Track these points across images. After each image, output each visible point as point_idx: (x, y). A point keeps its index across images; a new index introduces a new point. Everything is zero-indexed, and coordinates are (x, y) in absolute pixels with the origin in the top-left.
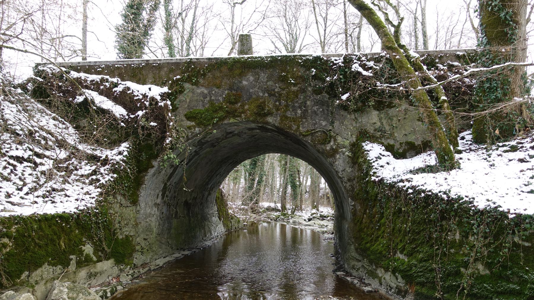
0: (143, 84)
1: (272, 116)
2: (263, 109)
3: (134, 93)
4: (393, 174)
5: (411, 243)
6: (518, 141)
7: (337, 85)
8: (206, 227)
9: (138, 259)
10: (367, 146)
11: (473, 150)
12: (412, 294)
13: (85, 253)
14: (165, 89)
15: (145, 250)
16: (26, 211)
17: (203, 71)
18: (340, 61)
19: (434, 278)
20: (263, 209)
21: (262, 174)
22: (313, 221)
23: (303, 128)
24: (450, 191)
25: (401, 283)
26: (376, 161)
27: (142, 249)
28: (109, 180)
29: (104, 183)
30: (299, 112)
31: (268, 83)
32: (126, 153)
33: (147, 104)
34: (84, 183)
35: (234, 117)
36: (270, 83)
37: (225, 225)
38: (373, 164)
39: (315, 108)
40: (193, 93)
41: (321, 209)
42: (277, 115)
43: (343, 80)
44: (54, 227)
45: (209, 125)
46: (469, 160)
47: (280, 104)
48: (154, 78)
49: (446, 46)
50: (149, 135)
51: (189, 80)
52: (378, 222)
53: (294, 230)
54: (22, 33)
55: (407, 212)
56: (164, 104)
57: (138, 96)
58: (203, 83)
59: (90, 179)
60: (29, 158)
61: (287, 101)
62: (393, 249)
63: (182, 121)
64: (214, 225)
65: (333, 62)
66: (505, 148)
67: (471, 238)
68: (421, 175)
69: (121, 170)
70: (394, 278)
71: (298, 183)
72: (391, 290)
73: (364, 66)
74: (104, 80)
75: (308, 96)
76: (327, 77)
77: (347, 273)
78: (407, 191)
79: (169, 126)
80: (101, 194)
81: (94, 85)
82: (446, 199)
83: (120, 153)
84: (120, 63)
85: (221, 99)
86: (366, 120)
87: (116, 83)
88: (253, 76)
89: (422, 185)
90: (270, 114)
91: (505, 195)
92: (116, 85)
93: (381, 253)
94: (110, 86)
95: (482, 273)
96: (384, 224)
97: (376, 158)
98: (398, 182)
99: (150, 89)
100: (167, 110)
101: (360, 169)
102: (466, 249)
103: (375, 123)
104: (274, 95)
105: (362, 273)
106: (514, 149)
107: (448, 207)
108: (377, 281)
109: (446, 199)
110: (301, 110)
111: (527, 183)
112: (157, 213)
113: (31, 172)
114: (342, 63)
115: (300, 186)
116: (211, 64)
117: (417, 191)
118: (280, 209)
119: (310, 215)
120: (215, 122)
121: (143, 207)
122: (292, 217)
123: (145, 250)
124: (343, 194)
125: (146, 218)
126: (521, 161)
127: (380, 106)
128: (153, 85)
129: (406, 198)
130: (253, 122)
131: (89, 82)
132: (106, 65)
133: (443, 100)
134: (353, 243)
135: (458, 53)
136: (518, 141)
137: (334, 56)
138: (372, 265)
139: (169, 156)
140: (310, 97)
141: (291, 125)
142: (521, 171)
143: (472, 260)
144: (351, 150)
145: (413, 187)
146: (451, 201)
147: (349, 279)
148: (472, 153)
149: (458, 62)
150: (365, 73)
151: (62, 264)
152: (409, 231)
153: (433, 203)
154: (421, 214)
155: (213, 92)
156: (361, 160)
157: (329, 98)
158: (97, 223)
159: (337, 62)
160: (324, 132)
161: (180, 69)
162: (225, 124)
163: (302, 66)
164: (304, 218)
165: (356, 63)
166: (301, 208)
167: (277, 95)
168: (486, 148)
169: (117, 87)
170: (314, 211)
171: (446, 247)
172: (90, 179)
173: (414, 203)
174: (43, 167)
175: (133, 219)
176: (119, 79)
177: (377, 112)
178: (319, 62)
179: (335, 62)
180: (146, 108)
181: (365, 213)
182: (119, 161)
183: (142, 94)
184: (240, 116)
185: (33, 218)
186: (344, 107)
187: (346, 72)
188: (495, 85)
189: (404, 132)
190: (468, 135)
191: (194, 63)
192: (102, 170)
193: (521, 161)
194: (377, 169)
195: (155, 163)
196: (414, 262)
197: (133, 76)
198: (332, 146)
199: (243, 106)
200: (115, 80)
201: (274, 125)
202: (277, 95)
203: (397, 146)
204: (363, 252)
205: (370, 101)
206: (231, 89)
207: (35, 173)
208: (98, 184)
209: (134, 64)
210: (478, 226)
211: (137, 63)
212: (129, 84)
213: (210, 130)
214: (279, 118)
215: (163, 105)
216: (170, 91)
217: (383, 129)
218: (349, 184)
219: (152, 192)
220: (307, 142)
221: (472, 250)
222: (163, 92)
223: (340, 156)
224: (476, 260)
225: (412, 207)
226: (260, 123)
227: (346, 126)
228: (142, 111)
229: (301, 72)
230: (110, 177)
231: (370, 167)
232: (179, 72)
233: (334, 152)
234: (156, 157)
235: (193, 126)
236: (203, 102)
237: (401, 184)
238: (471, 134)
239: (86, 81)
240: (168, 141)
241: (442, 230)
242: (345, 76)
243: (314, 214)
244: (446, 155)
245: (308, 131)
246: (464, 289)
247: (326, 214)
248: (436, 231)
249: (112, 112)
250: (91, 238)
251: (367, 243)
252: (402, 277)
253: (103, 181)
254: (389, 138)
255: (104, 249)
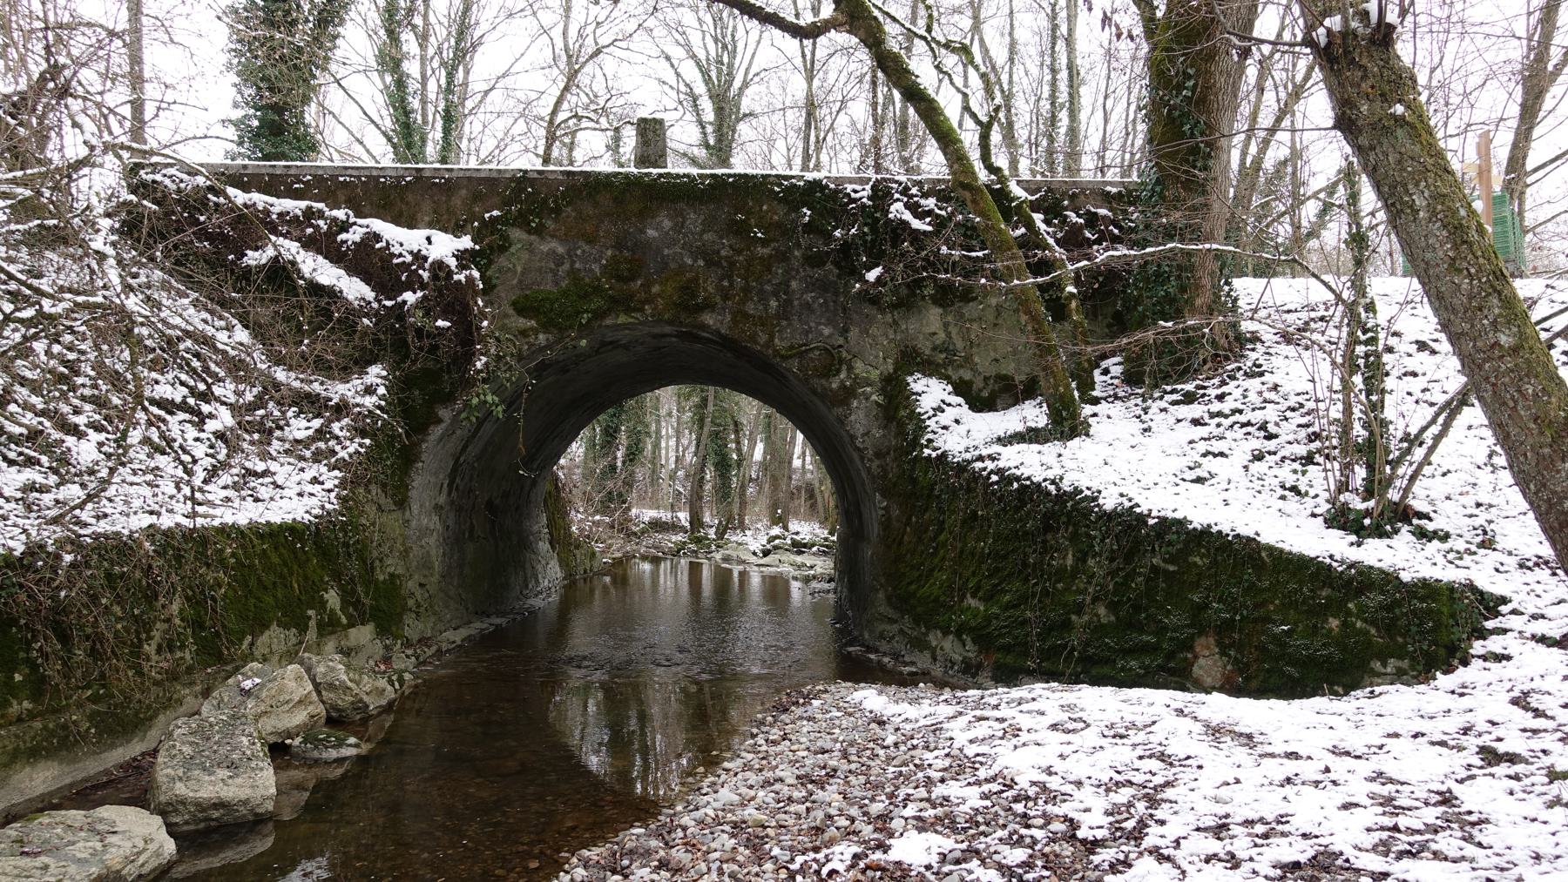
0: (411, 227)
1: (713, 311)
2: (694, 296)
3: (392, 249)
4: (965, 443)
5: (990, 576)
6: (1198, 382)
7: (857, 249)
8: (528, 565)
9: (413, 627)
10: (918, 383)
11: (1120, 398)
12: (989, 669)
13: (328, 606)
14: (466, 242)
15: (422, 610)
16: (242, 520)
17: (555, 202)
18: (865, 193)
19: (1027, 635)
20: (642, 526)
21: (639, 432)
22: (777, 556)
23: (782, 339)
24: (1061, 478)
25: (971, 651)
26: (934, 415)
27: (419, 606)
28: (357, 452)
29: (347, 457)
30: (773, 303)
31: (705, 237)
32: (382, 390)
33: (425, 275)
34: (302, 458)
35: (628, 311)
36: (708, 236)
37: (563, 563)
38: (928, 423)
39: (808, 297)
40: (531, 251)
41: (794, 526)
42: (724, 309)
43: (869, 238)
44: (283, 550)
45: (571, 327)
46: (1109, 417)
47: (731, 285)
48: (435, 212)
49: (1130, 94)
50: (434, 349)
51: (522, 221)
52: (934, 539)
53: (723, 577)
54: (157, 115)
55: (986, 519)
56: (466, 277)
57: (401, 255)
58: (554, 230)
59: (313, 448)
60: (184, 402)
61: (745, 279)
62: (960, 590)
63: (506, 316)
64: (543, 562)
65: (849, 195)
66: (1175, 397)
67: (1091, 562)
68: (1017, 447)
69: (378, 429)
70: (960, 645)
71: (735, 456)
72: (952, 668)
73: (914, 208)
74: (313, 213)
75: (793, 269)
76: (836, 228)
77: (868, 647)
78: (988, 477)
79: (479, 328)
80: (342, 484)
81: (289, 223)
82: (1054, 492)
83: (369, 390)
84: (349, 172)
85: (596, 268)
86: (918, 325)
87: (343, 222)
88: (670, 218)
89: (1017, 467)
90: (708, 306)
91: (1151, 485)
92: (345, 227)
93: (936, 600)
94: (330, 228)
95: (1104, 621)
96: (944, 544)
97: (934, 409)
98: (973, 461)
99: (429, 239)
100: (474, 291)
101: (902, 433)
102: (1080, 583)
103: (935, 334)
104: (718, 264)
105: (899, 645)
106: (1189, 398)
107: (1056, 508)
108: (927, 654)
109: (1054, 492)
110: (778, 300)
111: (1192, 465)
112: (438, 526)
113: (196, 434)
114: (869, 198)
115: (739, 463)
116: (573, 186)
117: (1006, 478)
118: (687, 524)
119: (764, 542)
120: (584, 322)
121: (416, 512)
122: (718, 546)
123: (422, 610)
124: (863, 484)
125: (420, 539)
126: (1196, 422)
127: (946, 296)
128: (434, 231)
129: (986, 493)
130: (670, 323)
131: (274, 217)
132: (314, 176)
133: (1070, 293)
134: (881, 585)
135: (1108, 188)
136: (1198, 382)
137: (851, 181)
138: (919, 625)
139: (482, 397)
140: (798, 272)
141: (756, 333)
142: (1190, 442)
143: (1088, 599)
144: (883, 391)
145: (999, 471)
146: (1061, 497)
147: (872, 656)
148: (1118, 404)
149: (1106, 208)
150: (916, 224)
151: (297, 626)
152: (989, 554)
153: (1032, 500)
154: (1012, 522)
155: (579, 252)
156: (903, 413)
157: (839, 276)
158: (346, 545)
159: (858, 195)
160: (826, 349)
161: (499, 194)
162: (607, 326)
163: (780, 200)
164: (752, 548)
165: (898, 200)
166: (742, 523)
167: (725, 264)
168: (1143, 396)
169: (348, 232)
170: (776, 531)
171: (1050, 579)
172: (313, 448)
173: (1000, 499)
174: (213, 421)
175: (400, 541)
176: (350, 212)
177: (940, 311)
178: (818, 194)
179: (853, 195)
180: (423, 286)
181: (908, 523)
182: (371, 408)
183: (411, 253)
184: (642, 310)
185: (253, 527)
186: (871, 297)
187: (878, 220)
188: (1167, 269)
189: (992, 354)
190: (1115, 365)
191: (532, 182)
192: (336, 427)
193: (1196, 422)
194: (935, 433)
195: (445, 413)
196: (995, 610)
197: (384, 207)
198: (842, 382)
199: (647, 286)
200: (340, 214)
201: (718, 332)
202: (725, 264)
203: (978, 383)
204: (902, 602)
205: (926, 287)
206: (619, 246)
207: (203, 435)
208: (333, 460)
209: (384, 177)
210: (1102, 541)
211: (393, 174)
212: (377, 225)
213: (572, 340)
214: (729, 317)
215: (463, 280)
216: (477, 247)
217: (951, 347)
218: (877, 462)
219: (433, 480)
220: (789, 370)
221: (1090, 583)
222: (462, 248)
223: (860, 403)
224: (1095, 599)
225: (996, 508)
226: (686, 326)
227: (874, 337)
228: (415, 292)
229: (779, 214)
230: (356, 445)
231: (921, 428)
232: (496, 200)
233: (848, 394)
234: (449, 399)
235: (532, 329)
236: (555, 275)
237: (978, 465)
238: (1119, 364)
239: (267, 212)
240: (479, 365)
241: (1045, 551)
242: (874, 230)
243: (777, 537)
244: (1064, 409)
245: (792, 347)
246: (1073, 649)
247: (808, 538)
248: (1035, 551)
249: (341, 292)
250: (337, 576)
251: (910, 584)
252: (974, 641)
253: (343, 454)
254: (962, 366)
255: (358, 601)
